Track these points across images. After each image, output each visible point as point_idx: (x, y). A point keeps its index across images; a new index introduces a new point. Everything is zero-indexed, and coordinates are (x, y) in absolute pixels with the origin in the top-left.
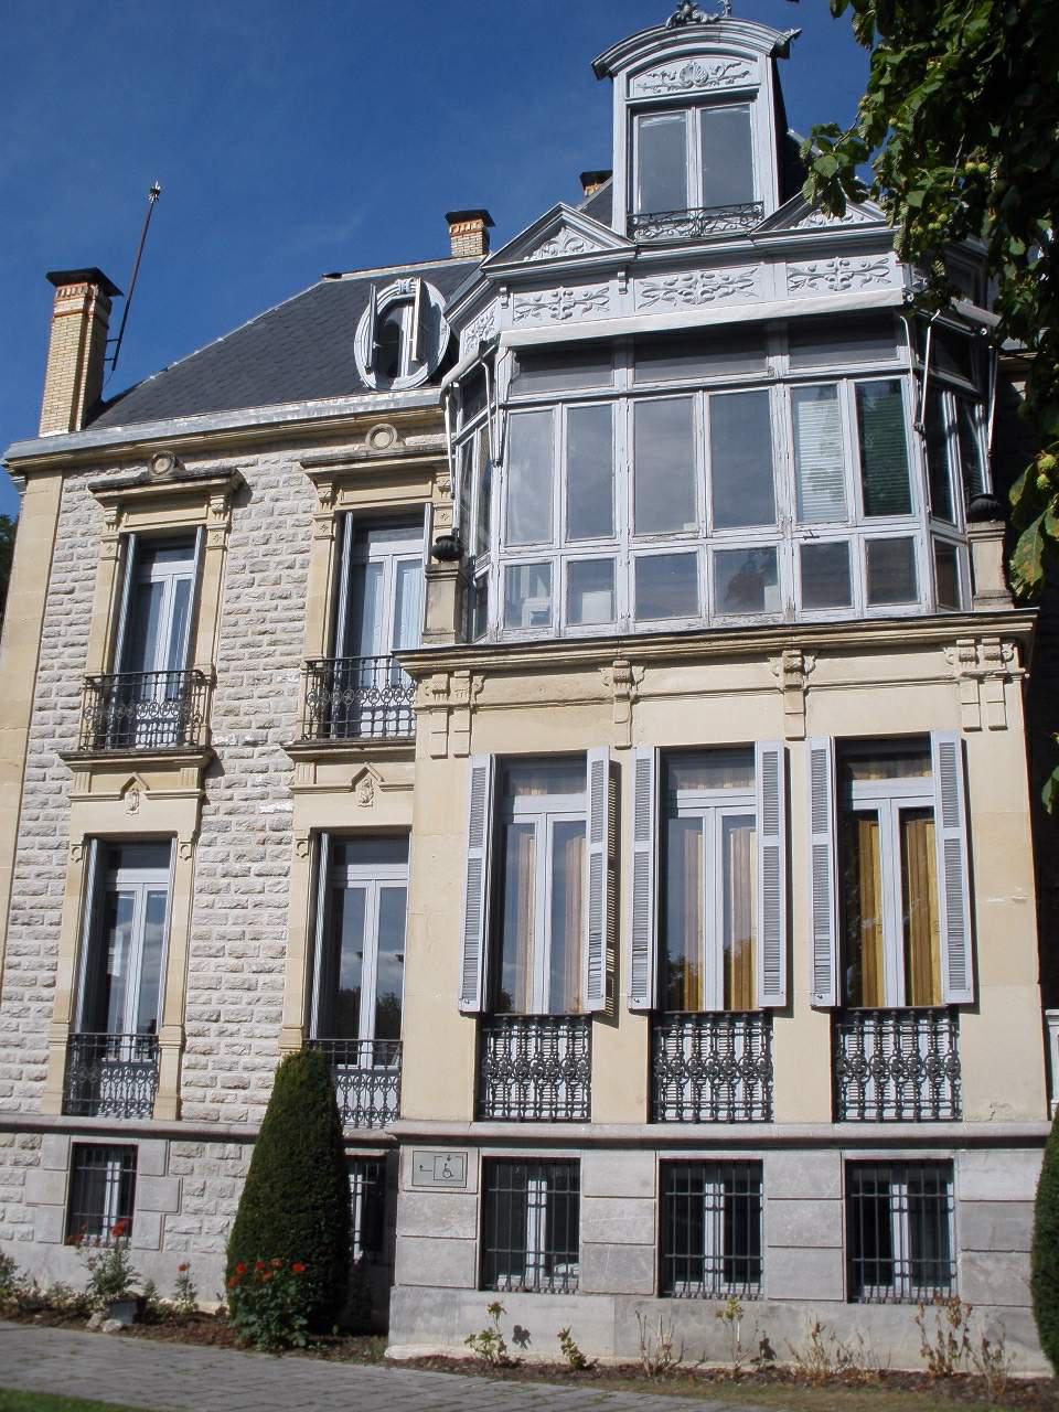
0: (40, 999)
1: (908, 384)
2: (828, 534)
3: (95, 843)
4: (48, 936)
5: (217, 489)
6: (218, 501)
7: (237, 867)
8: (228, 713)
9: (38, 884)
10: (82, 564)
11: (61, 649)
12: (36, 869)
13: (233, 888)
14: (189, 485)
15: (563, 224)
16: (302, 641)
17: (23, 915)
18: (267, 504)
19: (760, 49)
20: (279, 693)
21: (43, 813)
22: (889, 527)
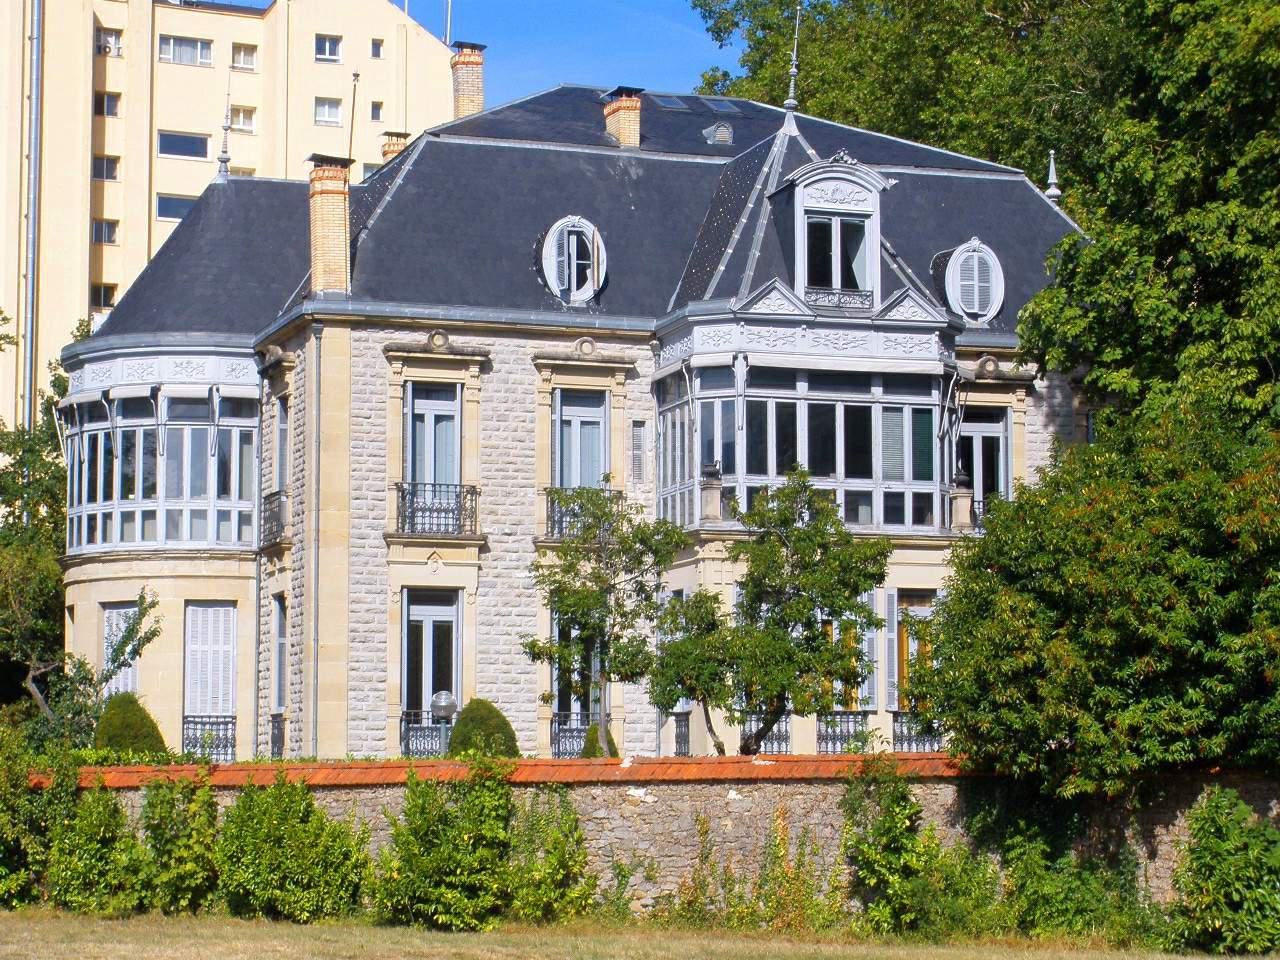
0: (376, 690)
1: (936, 412)
2: (896, 487)
3: (405, 590)
4: (379, 650)
5: (475, 363)
6: (475, 370)
7: (504, 610)
8: (491, 512)
9: (368, 616)
10: (375, 398)
11: (365, 458)
12: (366, 606)
13: (502, 623)
14: (458, 357)
15: (775, 288)
16: (534, 471)
17: (359, 636)
18: (502, 375)
19: (875, 187)
20: (523, 504)
21: (365, 570)
22: (923, 487)
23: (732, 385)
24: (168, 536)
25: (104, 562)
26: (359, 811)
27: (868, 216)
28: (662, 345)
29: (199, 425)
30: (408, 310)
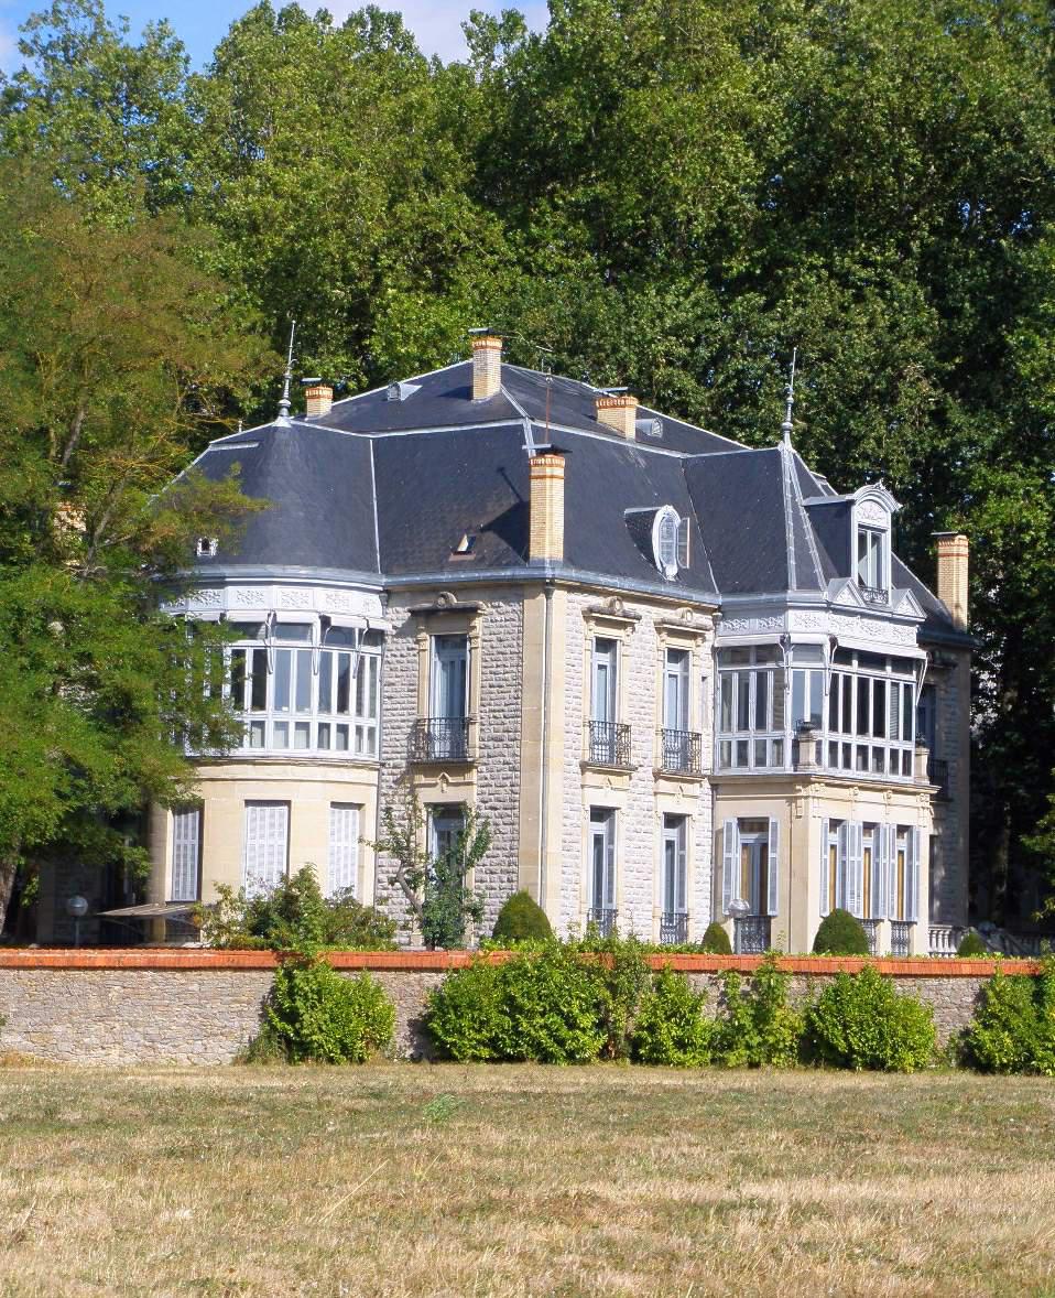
23: (821, 659)
24: (320, 745)
25: (255, 764)
26: (924, 993)
27: (884, 531)
28: (724, 618)
29: (346, 650)
30: (603, 579)
